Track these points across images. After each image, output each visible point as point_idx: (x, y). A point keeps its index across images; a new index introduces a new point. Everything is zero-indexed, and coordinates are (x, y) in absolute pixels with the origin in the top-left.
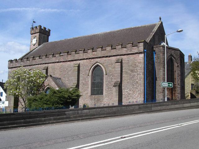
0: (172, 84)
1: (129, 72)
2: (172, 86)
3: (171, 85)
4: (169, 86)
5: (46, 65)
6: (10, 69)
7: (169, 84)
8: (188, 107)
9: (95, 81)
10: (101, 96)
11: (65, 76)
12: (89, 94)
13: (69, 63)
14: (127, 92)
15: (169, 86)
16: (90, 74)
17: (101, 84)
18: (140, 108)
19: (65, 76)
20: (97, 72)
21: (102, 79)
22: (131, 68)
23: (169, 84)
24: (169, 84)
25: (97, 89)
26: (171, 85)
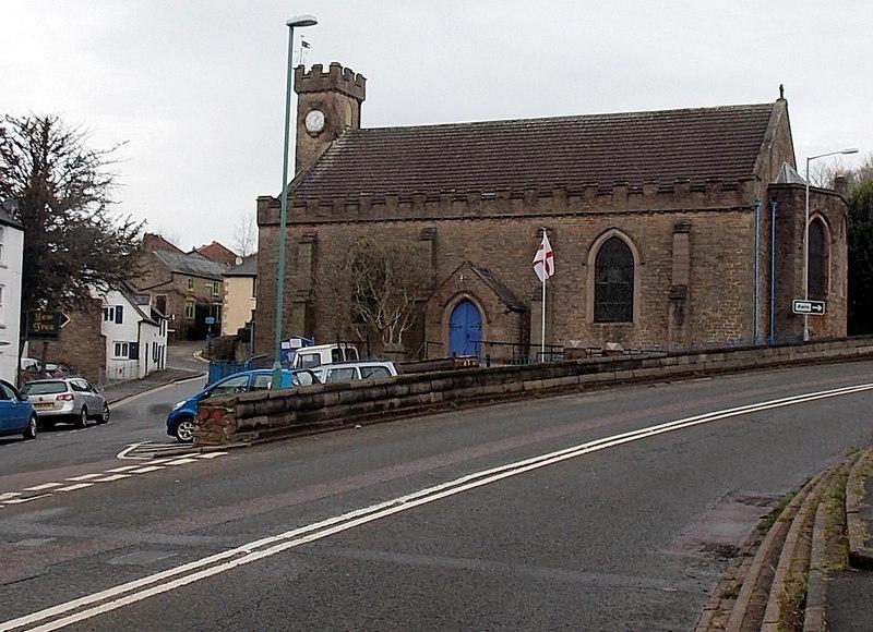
0: (821, 305)
1: (713, 260)
2: (821, 311)
3: (819, 308)
4: (813, 311)
5: (428, 224)
6: (268, 229)
7: (813, 305)
8: (833, 359)
9: (606, 280)
10: (628, 326)
11: (504, 262)
12: (590, 317)
13: (514, 223)
14: (704, 314)
15: (813, 311)
16: (591, 260)
17: (627, 292)
18: (261, 436)
19: (504, 262)
20: (614, 259)
21: (629, 277)
22: (717, 249)
23: (813, 305)
24: (816, 305)
25: (613, 303)
26: (819, 308)
